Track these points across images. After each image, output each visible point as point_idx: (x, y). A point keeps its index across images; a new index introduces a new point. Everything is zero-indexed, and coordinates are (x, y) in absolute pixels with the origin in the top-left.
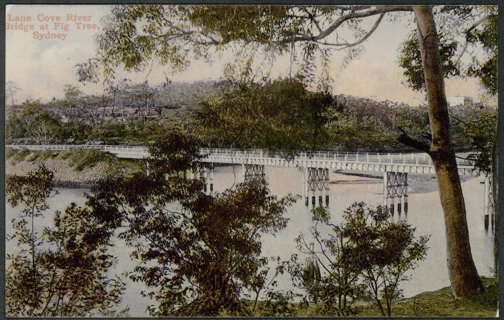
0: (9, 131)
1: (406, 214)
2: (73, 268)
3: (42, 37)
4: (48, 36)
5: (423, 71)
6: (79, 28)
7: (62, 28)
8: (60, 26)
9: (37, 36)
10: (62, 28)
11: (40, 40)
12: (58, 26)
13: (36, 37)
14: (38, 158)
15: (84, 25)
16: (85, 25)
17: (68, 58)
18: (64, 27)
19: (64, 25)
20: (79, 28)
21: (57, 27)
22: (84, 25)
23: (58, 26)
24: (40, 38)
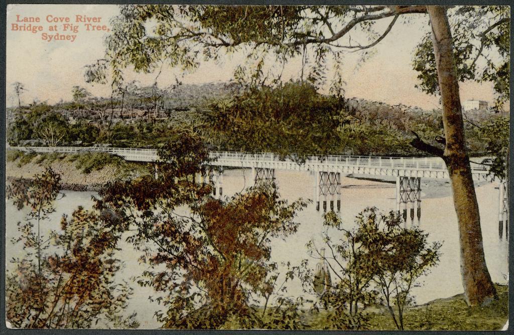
3: (51, 38)
4: (56, 37)
6: (88, 29)
10: (72, 30)
13: (45, 38)
18: (73, 28)
19: (73, 26)
20: (88, 29)
21: (66, 28)
23: (67, 27)
24: (49, 39)
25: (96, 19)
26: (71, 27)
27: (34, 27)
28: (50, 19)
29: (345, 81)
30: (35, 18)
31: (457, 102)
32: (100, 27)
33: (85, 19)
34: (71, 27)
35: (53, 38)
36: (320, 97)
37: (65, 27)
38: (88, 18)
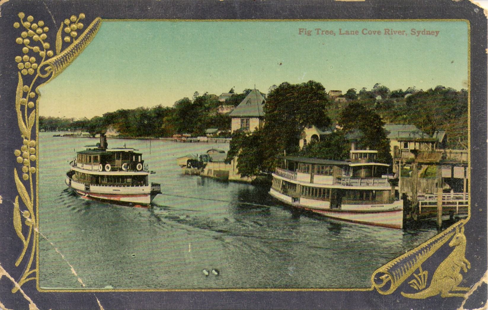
0: (42, 42)
1: (64, 136)
2: (62, 128)
3: (419, 34)
4: (423, 33)
5: (443, 215)
6: (318, 34)
7: (306, 34)
8: (304, 32)
9: (415, 32)
10: (306, 34)
11: (417, 36)
12: (303, 32)
13: (414, 33)
14: (246, 238)
15: (323, 31)
16: (324, 31)
17: (282, 63)
18: (307, 33)
19: (307, 30)
20: (318, 34)
21: (301, 33)
22: (323, 31)
23: (303, 32)
24: (417, 34)
25: (401, 32)
26: (306, 32)
27: (308, 31)
28: (365, 32)
29: (206, 151)
30: (355, 31)
31: (473, 163)
32: (328, 32)
33: (392, 31)
34: (306, 32)
35: (421, 34)
36: (395, 248)
37: (300, 31)
38: (394, 32)
